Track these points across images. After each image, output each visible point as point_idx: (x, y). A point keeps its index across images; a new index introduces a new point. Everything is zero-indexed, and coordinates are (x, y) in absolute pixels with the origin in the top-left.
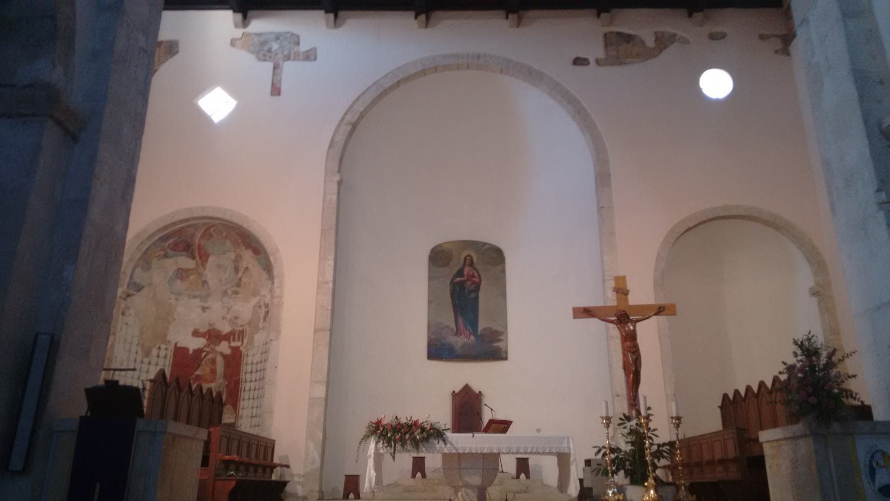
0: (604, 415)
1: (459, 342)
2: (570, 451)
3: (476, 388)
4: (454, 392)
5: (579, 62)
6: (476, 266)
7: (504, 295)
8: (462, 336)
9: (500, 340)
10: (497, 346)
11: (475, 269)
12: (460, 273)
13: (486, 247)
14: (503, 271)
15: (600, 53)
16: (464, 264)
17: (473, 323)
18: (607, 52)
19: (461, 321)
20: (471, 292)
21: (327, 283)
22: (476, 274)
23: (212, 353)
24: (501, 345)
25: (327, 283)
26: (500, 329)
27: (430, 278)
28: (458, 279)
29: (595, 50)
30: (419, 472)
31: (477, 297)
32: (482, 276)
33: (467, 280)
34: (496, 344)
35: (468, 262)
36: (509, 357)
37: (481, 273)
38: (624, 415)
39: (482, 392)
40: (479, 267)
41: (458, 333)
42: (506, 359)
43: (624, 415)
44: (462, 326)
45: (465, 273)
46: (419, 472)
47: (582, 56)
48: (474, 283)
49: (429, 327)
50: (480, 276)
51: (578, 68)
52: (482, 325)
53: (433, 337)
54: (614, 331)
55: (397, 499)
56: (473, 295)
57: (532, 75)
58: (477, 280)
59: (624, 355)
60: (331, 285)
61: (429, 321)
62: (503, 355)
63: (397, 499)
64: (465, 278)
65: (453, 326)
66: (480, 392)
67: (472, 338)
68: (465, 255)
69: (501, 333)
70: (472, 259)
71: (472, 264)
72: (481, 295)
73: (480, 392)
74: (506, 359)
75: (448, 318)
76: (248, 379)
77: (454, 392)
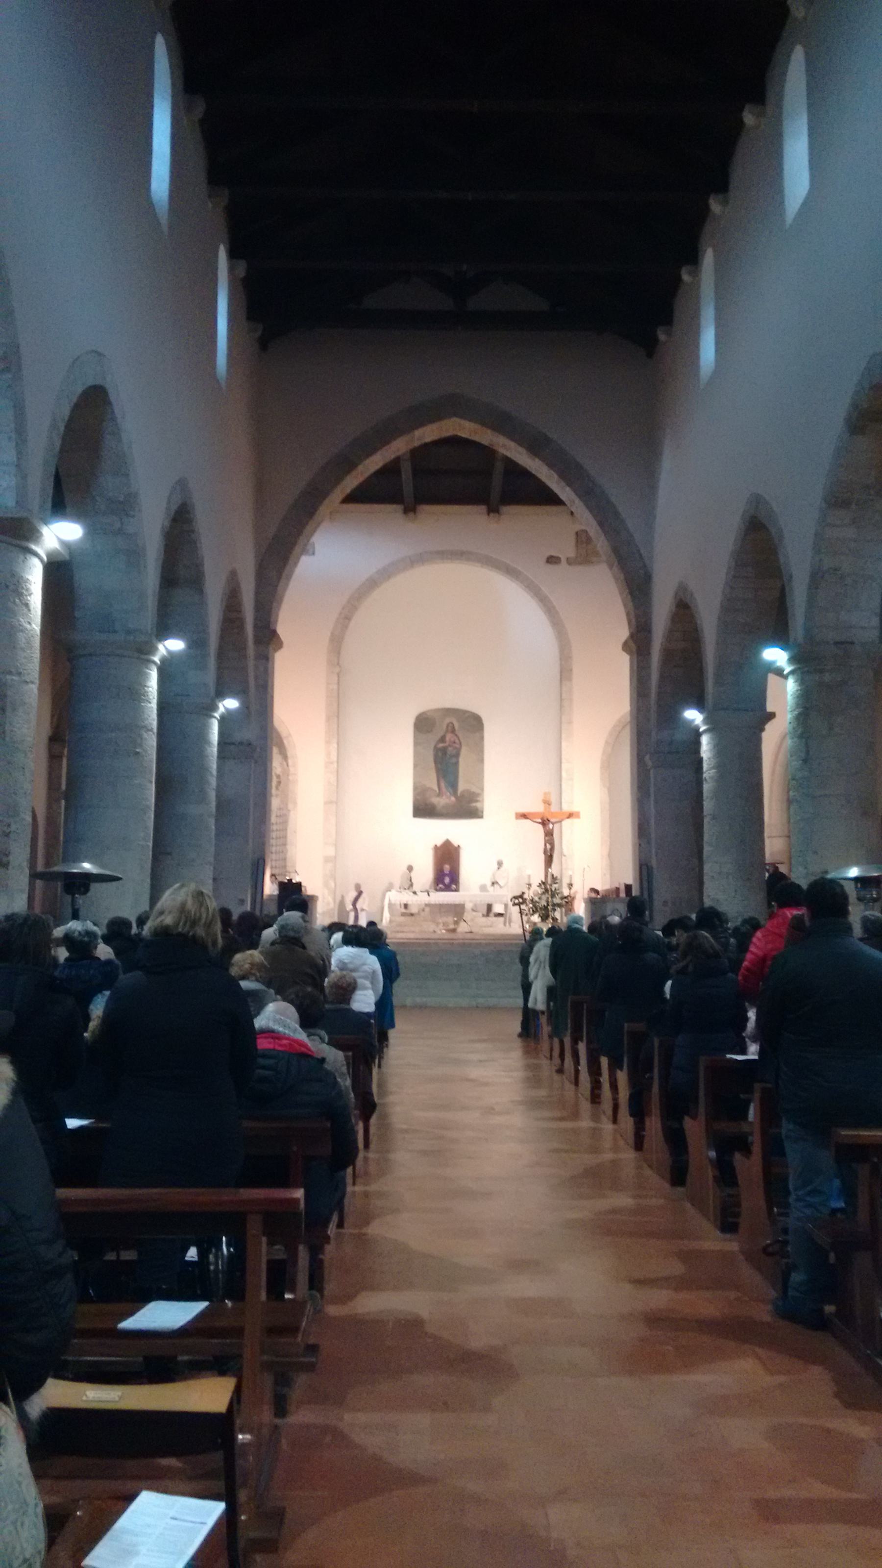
0: (527, 882)
1: (443, 801)
2: (255, 910)
4: (436, 846)
5: (552, 560)
6: (457, 732)
7: (481, 761)
9: (477, 801)
10: (474, 807)
11: (456, 735)
12: (443, 739)
13: (467, 715)
15: (572, 553)
16: (447, 731)
17: (453, 785)
18: (577, 550)
19: (443, 784)
20: (452, 756)
21: (332, 763)
22: (457, 741)
24: (478, 805)
25: (332, 763)
26: (477, 791)
27: (416, 744)
29: (567, 549)
31: (457, 763)
34: (474, 804)
35: (450, 728)
36: (484, 817)
37: (462, 740)
38: (542, 882)
39: (460, 845)
40: (460, 736)
41: (440, 795)
42: (481, 817)
43: (542, 882)
45: (447, 739)
48: (456, 748)
50: (460, 743)
51: (550, 567)
52: (462, 786)
53: (418, 797)
55: (52, 532)
56: (454, 760)
57: (511, 572)
58: (457, 746)
62: (480, 814)
63: (52, 532)
64: (447, 744)
66: (459, 846)
67: (453, 799)
68: (449, 722)
69: (478, 795)
70: (453, 727)
71: (453, 731)
72: (461, 760)
74: (481, 817)
75: (431, 781)
76: (274, 844)
77: (436, 846)
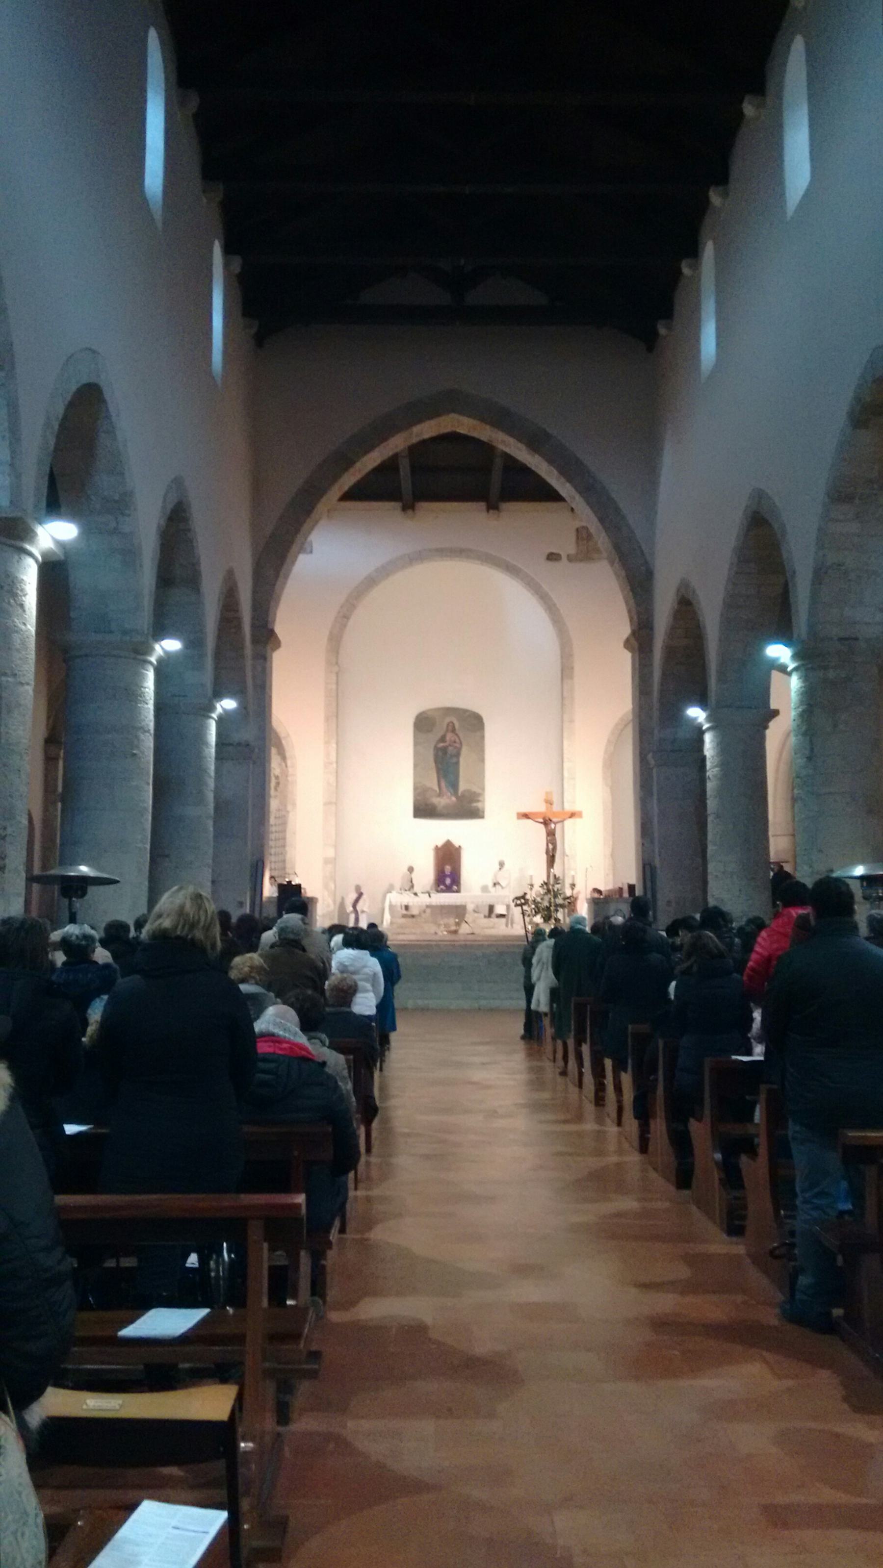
1: (443, 801)
3: (456, 843)
4: (437, 846)
5: (552, 557)
6: (457, 732)
7: (482, 760)
8: (445, 797)
9: (478, 801)
11: (457, 735)
12: (443, 739)
13: (468, 714)
14: (483, 737)
15: (572, 549)
16: (447, 730)
19: (443, 784)
20: (452, 756)
21: (331, 763)
22: (457, 740)
23: (620, 1133)
24: (479, 805)
26: (478, 791)
27: (416, 744)
28: (441, 745)
29: (568, 547)
30: (224, 1460)
31: (457, 763)
32: (463, 743)
33: (450, 745)
34: (475, 804)
35: (450, 728)
37: (462, 740)
39: (461, 845)
40: (461, 735)
41: (440, 795)
42: (482, 817)
44: (444, 789)
45: (448, 738)
46: (224, 1460)
47: (554, 551)
48: (456, 747)
49: (415, 789)
50: (461, 743)
51: (551, 564)
52: (463, 786)
54: (542, 829)
56: (454, 760)
58: (457, 745)
59: (547, 845)
60: (335, 765)
61: (415, 784)
62: (481, 814)
65: (437, 788)
66: (460, 847)
67: (454, 799)
70: (454, 727)
71: (453, 730)
72: (462, 760)
73: (460, 847)
74: (482, 817)
75: (432, 781)
